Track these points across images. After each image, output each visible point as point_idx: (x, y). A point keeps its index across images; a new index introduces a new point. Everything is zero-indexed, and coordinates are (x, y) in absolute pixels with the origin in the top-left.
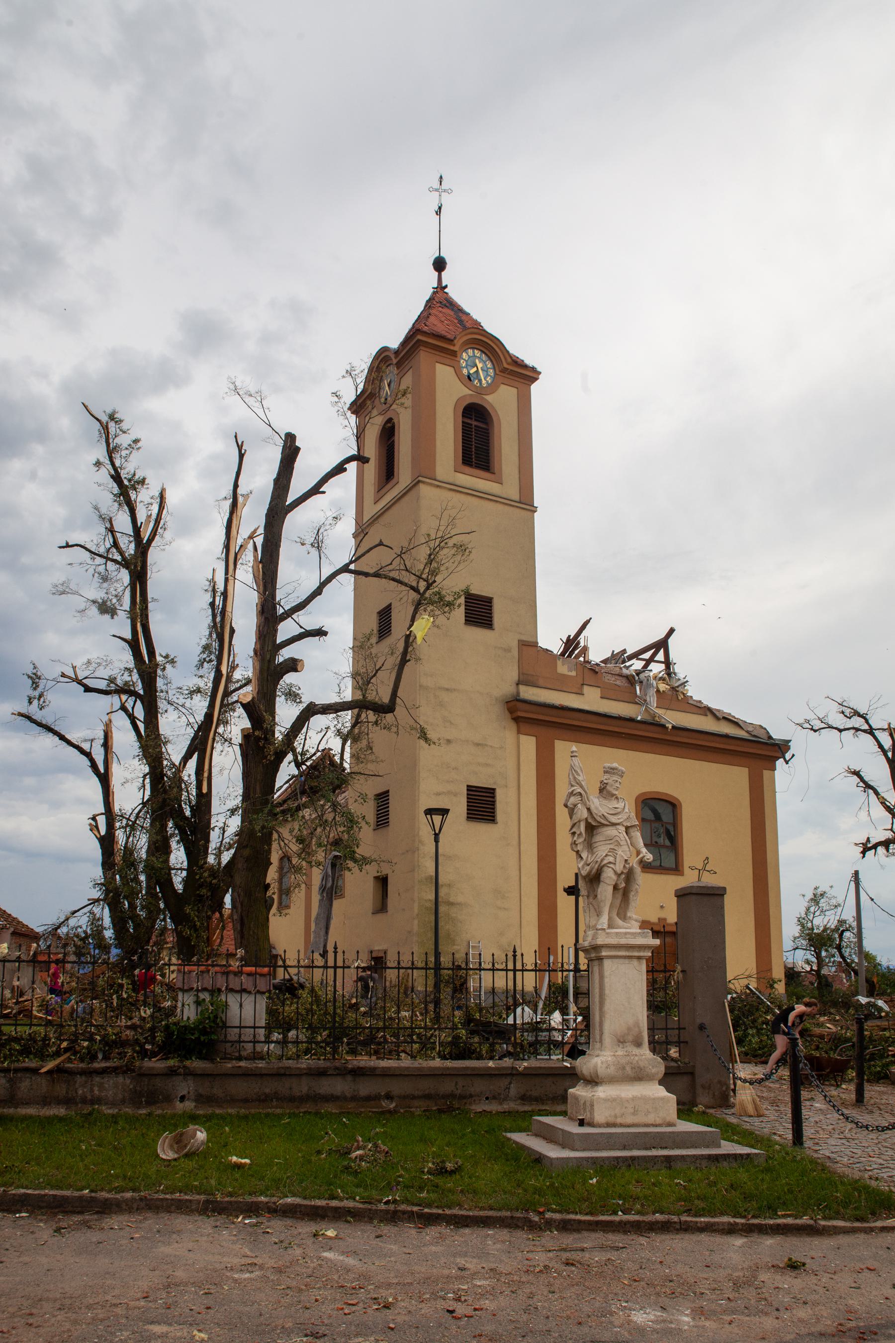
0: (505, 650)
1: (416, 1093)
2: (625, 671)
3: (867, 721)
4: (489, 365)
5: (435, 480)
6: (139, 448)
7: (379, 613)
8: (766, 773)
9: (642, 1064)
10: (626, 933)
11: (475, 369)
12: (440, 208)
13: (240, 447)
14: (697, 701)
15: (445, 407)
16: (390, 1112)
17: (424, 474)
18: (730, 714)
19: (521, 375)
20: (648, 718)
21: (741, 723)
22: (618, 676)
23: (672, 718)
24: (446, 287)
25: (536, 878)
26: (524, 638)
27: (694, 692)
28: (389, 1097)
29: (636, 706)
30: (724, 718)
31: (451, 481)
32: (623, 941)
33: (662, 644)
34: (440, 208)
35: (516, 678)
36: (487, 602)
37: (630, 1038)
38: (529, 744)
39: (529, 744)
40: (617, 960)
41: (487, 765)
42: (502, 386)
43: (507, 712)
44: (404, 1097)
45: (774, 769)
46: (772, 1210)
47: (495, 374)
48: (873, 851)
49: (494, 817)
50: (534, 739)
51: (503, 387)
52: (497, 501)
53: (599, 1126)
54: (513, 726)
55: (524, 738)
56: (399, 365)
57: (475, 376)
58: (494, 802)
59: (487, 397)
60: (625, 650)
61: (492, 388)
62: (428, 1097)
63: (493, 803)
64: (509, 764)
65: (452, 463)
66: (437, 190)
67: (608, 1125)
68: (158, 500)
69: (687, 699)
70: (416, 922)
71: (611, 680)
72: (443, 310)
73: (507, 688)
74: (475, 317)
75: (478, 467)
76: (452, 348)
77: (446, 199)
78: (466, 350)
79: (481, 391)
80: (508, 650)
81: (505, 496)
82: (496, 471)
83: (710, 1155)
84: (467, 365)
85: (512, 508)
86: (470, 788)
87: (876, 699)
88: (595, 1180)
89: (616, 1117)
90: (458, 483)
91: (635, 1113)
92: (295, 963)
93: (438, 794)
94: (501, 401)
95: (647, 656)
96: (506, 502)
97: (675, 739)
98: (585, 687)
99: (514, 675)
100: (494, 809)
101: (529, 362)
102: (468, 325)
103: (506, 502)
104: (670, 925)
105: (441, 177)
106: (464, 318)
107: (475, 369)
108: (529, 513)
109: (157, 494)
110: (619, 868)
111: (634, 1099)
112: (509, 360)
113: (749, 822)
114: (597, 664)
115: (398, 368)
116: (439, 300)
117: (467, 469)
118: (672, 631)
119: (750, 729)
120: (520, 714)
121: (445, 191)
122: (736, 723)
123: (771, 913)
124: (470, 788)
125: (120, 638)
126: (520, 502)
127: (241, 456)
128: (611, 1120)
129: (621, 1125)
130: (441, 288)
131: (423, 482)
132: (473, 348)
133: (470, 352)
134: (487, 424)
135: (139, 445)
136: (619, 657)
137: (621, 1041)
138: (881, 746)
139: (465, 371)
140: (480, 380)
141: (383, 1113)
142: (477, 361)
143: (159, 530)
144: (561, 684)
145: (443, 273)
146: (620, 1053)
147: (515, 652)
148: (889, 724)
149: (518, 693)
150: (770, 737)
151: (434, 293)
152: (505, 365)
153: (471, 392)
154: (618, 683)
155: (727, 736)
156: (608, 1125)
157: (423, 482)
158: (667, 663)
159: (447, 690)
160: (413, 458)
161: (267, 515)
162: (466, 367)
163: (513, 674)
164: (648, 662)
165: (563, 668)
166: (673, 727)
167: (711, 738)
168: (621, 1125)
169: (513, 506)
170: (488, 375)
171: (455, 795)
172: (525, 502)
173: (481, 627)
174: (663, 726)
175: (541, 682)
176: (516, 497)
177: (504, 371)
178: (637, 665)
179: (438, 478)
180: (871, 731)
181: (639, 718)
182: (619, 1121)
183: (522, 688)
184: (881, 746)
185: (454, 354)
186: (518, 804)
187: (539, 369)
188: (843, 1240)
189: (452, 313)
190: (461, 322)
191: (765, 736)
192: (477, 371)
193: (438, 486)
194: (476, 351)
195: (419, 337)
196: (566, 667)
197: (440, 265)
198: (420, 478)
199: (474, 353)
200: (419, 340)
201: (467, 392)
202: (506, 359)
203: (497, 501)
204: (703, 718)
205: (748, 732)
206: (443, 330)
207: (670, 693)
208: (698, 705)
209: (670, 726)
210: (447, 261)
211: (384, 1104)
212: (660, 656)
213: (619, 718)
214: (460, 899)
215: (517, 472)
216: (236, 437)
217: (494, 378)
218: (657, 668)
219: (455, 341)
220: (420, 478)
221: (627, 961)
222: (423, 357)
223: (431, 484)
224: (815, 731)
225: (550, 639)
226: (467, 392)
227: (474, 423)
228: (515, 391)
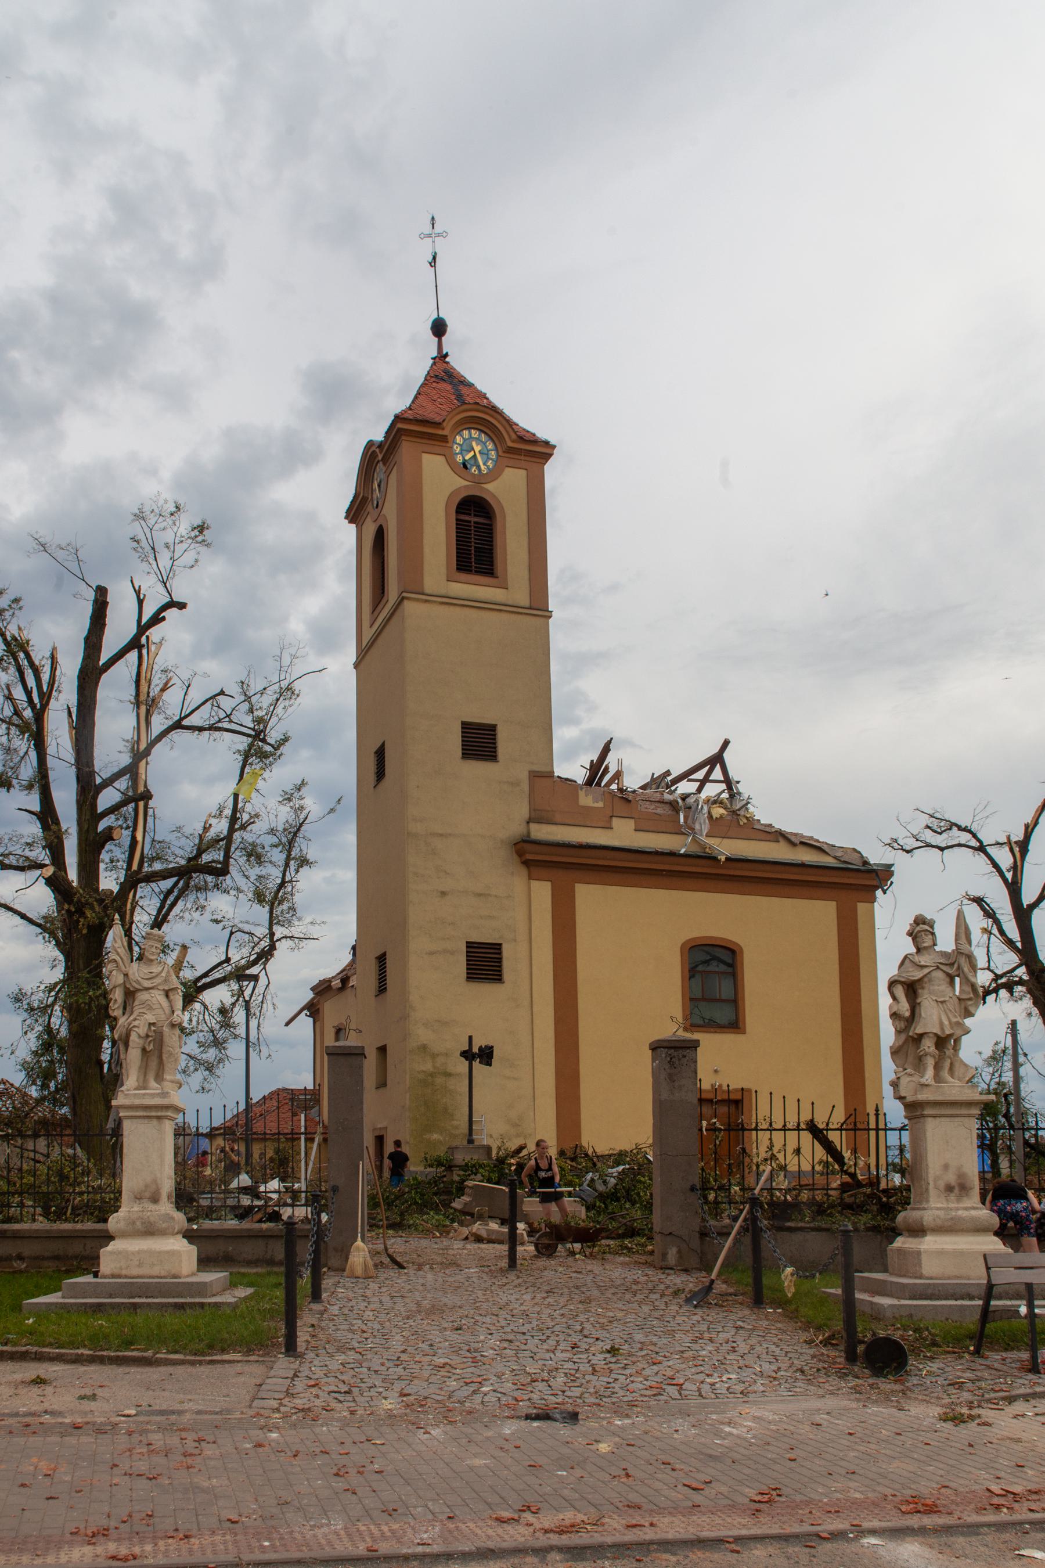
0: (512, 784)
1: (47, 1254)
2: (667, 797)
3: (974, 836)
4: (490, 446)
5: (423, 594)
6: (20, 608)
7: (376, 753)
8: (861, 907)
9: (152, 1219)
10: (144, 1094)
11: (472, 453)
12: (434, 258)
13: (138, 593)
14: (765, 825)
15: (453, 501)
16: (21, 1272)
17: (413, 589)
18: (812, 838)
19: (531, 452)
20: (695, 849)
21: (825, 847)
22: (661, 801)
23: (725, 848)
24: (447, 355)
26: (536, 768)
27: (763, 813)
28: (20, 1258)
29: (683, 837)
30: (802, 843)
31: (443, 592)
32: (137, 1102)
33: (717, 759)
34: (434, 258)
35: (527, 816)
36: (490, 730)
37: (147, 1194)
39: (542, 891)
40: (135, 1120)
42: (508, 470)
43: (515, 856)
44: (36, 1258)
45: (873, 900)
46: (128, 1344)
47: (498, 456)
48: (994, 995)
49: (500, 975)
50: (549, 884)
51: (508, 471)
52: (500, 610)
53: (105, 1277)
54: (524, 871)
55: (535, 884)
56: (385, 460)
57: (472, 462)
58: (501, 959)
59: (489, 487)
60: (668, 771)
61: (494, 474)
62: (56, 1258)
63: (500, 960)
64: (521, 913)
65: (444, 570)
66: (429, 236)
67: (113, 1276)
68: (49, 662)
69: (751, 820)
70: (408, 1096)
71: (651, 808)
72: (438, 386)
73: (516, 828)
74: (479, 388)
75: (479, 572)
76: (440, 432)
77: (441, 246)
78: (459, 433)
79: (480, 479)
80: (515, 784)
81: (510, 603)
83: (176, 1303)
84: (462, 450)
85: (520, 616)
86: (470, 945)
87: (981, 807)
88: (31, 1321)
89: (121, 1268)
90: (452, 594)
91: (140, 1265)
93: (431, 953)
94: (506, 489)
95: (700, 775)
96: (513, 609)
97: (732, 872)
98: (614, 819)
99: (524, 812)
100: (500, 966)
101: (542, 434)
102: (468, 400)
103: (513, 609)
104: (707, 1091)
105: (433, 218)
106: (464, 390)
107: (472, 453)
108: (542, 620)
109: (48, 654)
110: (143, 1030)
111: (139, 1252)
112: (514, 436)
113: (837, 966)
114: (634, 791)
115: (384, 464)
116: (443, 375)
117: (464, 576)
118: (726, 743)
119: (839, 854)
120: (529, 857)
121: (439, 235)
122: (818, 848)
123: (867, 1075)
124: (470, 945)
125: (26, 810)
126: (530, 608)
128: (116, 1272)
129: (126, 1277)
130: (442, 357)
131: (408, 598)
132: (470, 429)
133: (466, 433)
135: (21, 603)
136: (661, 782)
137: (138, 1198)
138: (995, 865)
139: (459, 459)
140: (478, 467)
141: (15, 1272)
142: (474, 444)
143: (54, 693)
144: (585, 818)
146: (136, 1209)
147: (525, 786)
148: (1008, 838)
149: (529, 833)
150: (866, 863)
151: (434, 364)
152: (510, 444)
154: (659, 811)
155: (803, 865)
156: (113, 1276)
157: (408, 598)
158: (728, 781)
159: (441, 835)
160: (399, 573)
161: (79, 677)
162: (461, 453)
163: (523, 811)
164: (703, 782)
165: (586, 799)
166: (728, 859)
167: (632, 856)
168: (126, 1277)
169: (521, 613)
170: (489, 459)
171: (452, 953)
172: (538, 607)
173: (481, 760)
174: (715, 859)
175: (558, 818)
176: (526, 603)
177: (510, 451)
178: (686, 787)
179: (427, 591)
180: (981, 849)
181: (682, 851)
182: (124, 1272)
183: (533, 827)
184: (995, 865)
185: (444, 439)
186: (530, 961)
187: (553, 442)
188: (180, 1370)
189: (449, 387)
190: (459, 397)
191: (859, 862)
192: (475, 456)
193: (426, 601)
194: (473, 432)
195: (399, 425)
196: (590, 797)
197: (439, 328)
198: (404, 594)
199: (470, 434)
200: (399, 430)
202: (510, 437)
203: (500, 610)
204: (773, 845)
205: (835, 858)
206: (447, 409)
207: (728, 818)
208: (768, 829)
209: (723, 858)
210: (448, 323)
211: (15, 1264)
212: (717, 774)
213: (657, 853)
215: (526, 572)
216: (132, 581)
217: (496, 462)
218: (711, 790)
219: (444, 424)
220: (404, 594)
221: (146, 1121)
222: (406, 448)
223: (418, 600)
224: (908, 852)
225: (572, 768)
228: (523, 473)
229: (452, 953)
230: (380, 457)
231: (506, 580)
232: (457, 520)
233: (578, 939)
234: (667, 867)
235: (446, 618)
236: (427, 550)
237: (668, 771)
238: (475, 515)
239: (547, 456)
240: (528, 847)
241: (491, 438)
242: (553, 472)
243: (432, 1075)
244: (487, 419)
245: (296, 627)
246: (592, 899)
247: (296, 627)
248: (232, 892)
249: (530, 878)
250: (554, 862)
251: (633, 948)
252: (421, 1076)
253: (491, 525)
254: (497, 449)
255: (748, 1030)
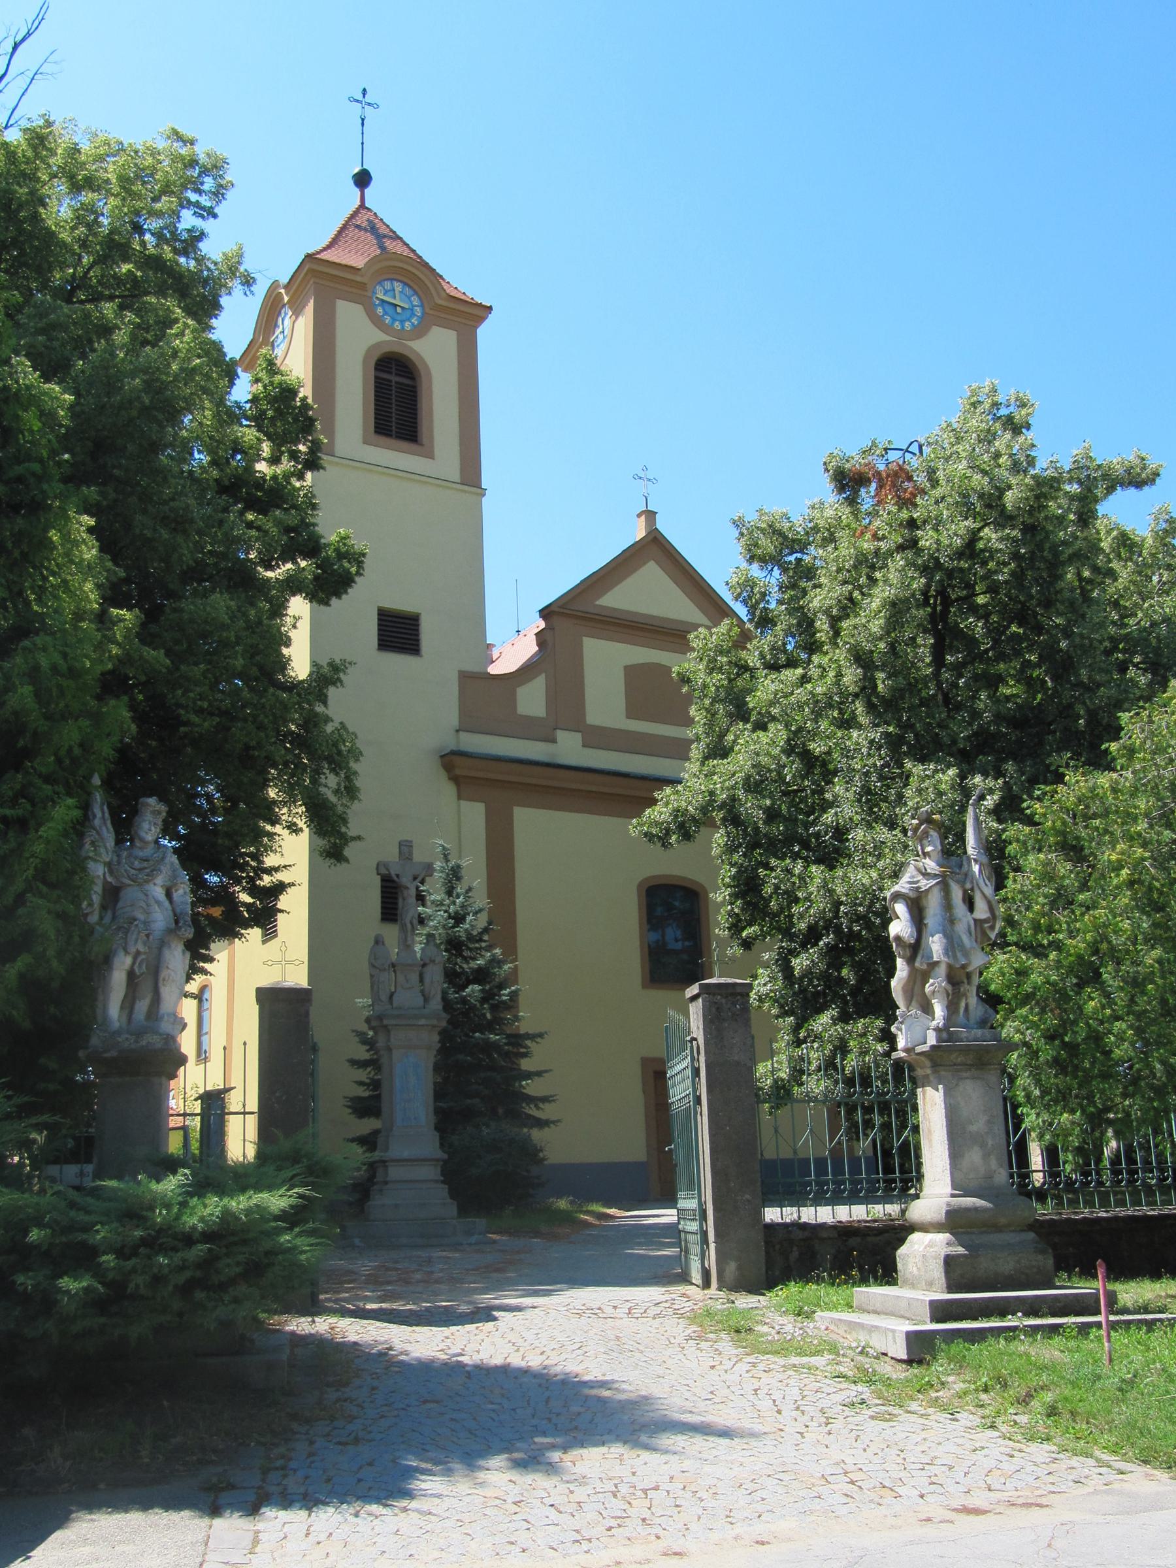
39: (475, 813)
47: (424, 313)
51: (436, 330)
54: (450, 789)
55: (465, 804)
60: (646, 1062)
76: (358, 279)
82: (425, 440)
92: (239, 1108)
94: (434, 351)
116: (363, 223)
117: (383, 440)
120: (458, 772)
121: (369, 104)
132: (392, 280)
134: (413, 379)
145: (287, 882)
153: (388, 338)
172: (470, 475)
183: (463, 735)
197: (363, 179)
201: (384, 337)
226: (384, 337)
227: (394, 378)
230: (286, 299)
231: (432, 452)
232: (376, 377)
237: (646, 1062)
238: (397, 375)
239: (482, 319)
241: (416, 293)
242: (484, 333)
244: (415, 274)
246: (530, 823)
249: (460, 797)
253: (415, 387)
254: (422, 306)
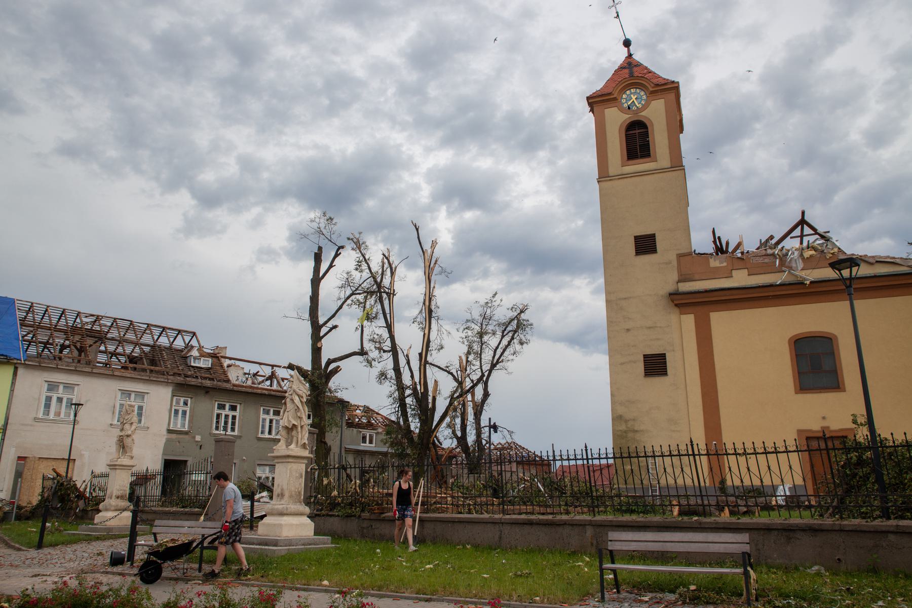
0: (666, 263)
4: (642, 93)
18: (888, 257)
20: (791, 279)
21: (898, 261)
25: (701, 407)
31: (620, 173)
33: (803, 222)
38: (689, 321)
39: (689, 321)
41: (658, 339)
54: (677, 310)
55: (684, 317)
64: (678, 336)
71: (760, 260)
73: (671, 288)
75: (642, 157)
78: (624, 93)
86: (645, 356)
93: (622, 364)
94: (655, 113)
99: (675, 277)
118: (803, 213)
120: (676, 302)
124: (645, 356)
127: (417, 230)
139: (626, 105)
144: (715, 274)
147: (675, 263)
154: (766, 261)
164: (802, 236)
167: (744, 291)
171: (635, 362)
177: (652, 92)
179: (611, 174)
183: (680, 285)
187: (676, 80)
197: (627, 43)
209: (808, 282)
214: (642, 428)
226: (628, 116)
229: (635, 362)
233: (714, 344)
234: (772, 294)
235: (642, 180)
236: (609, 155)
240: (675, 297)
243: (625, 432)
245: (855, 137)
246: (722, 322)
247: (855, 137)
248: (128, 430)
250: (690, 302)
251: (755, 345)
252: (619, 433)
255: (847, 389)
